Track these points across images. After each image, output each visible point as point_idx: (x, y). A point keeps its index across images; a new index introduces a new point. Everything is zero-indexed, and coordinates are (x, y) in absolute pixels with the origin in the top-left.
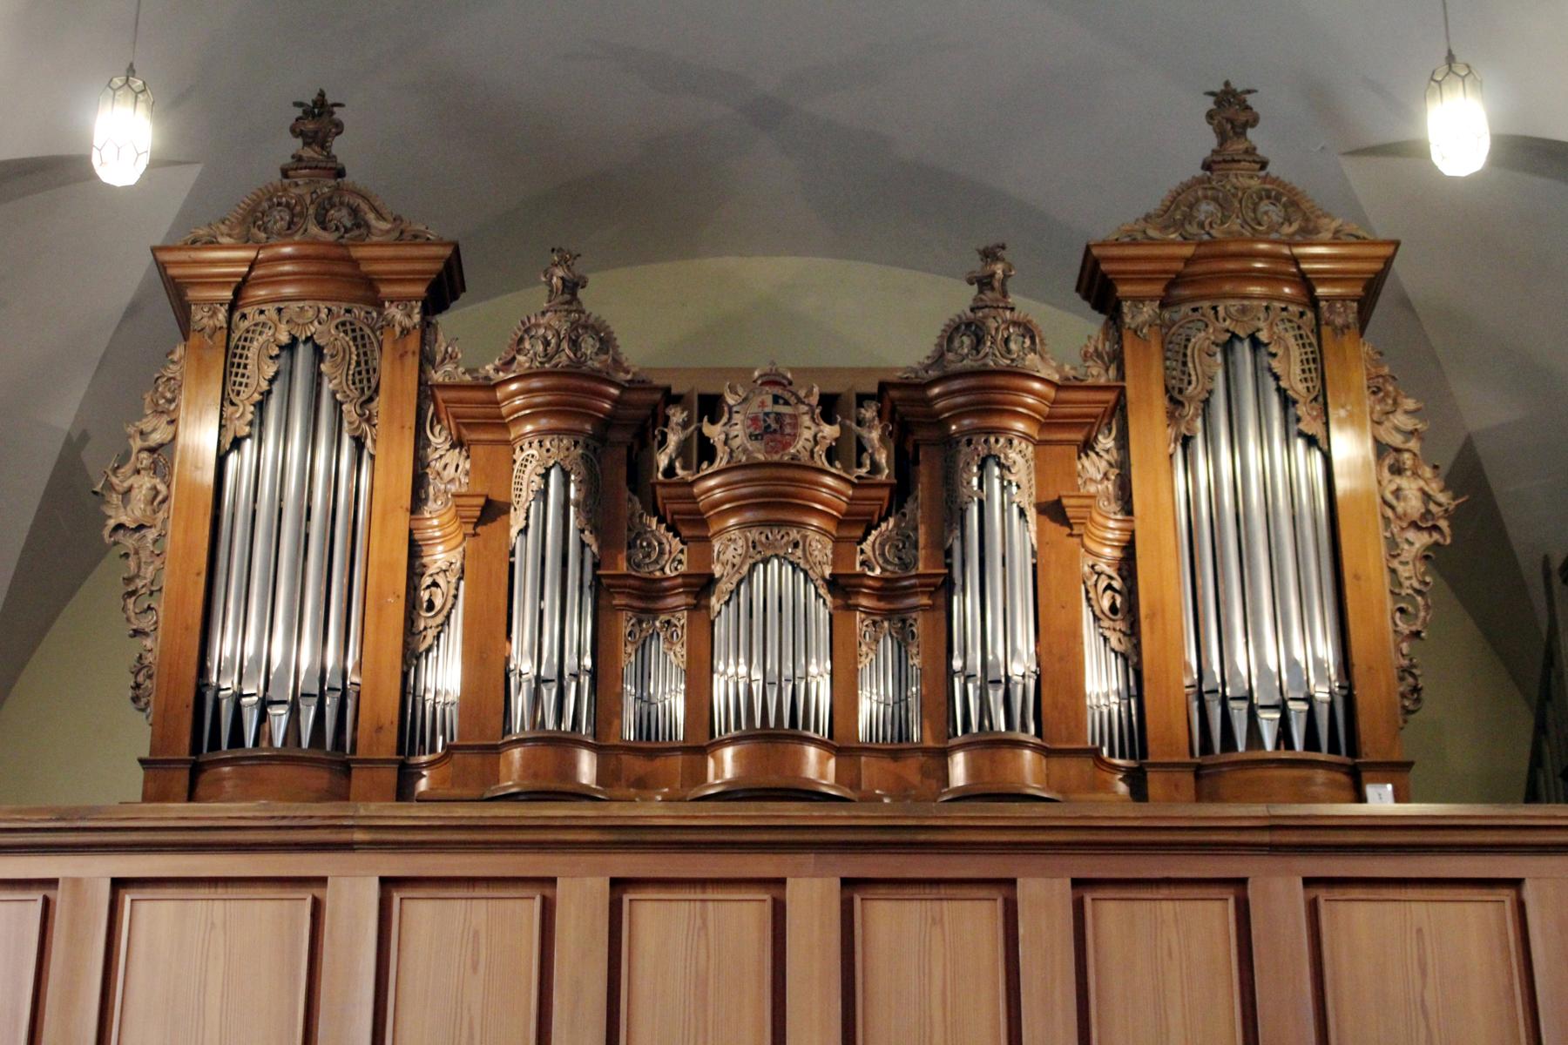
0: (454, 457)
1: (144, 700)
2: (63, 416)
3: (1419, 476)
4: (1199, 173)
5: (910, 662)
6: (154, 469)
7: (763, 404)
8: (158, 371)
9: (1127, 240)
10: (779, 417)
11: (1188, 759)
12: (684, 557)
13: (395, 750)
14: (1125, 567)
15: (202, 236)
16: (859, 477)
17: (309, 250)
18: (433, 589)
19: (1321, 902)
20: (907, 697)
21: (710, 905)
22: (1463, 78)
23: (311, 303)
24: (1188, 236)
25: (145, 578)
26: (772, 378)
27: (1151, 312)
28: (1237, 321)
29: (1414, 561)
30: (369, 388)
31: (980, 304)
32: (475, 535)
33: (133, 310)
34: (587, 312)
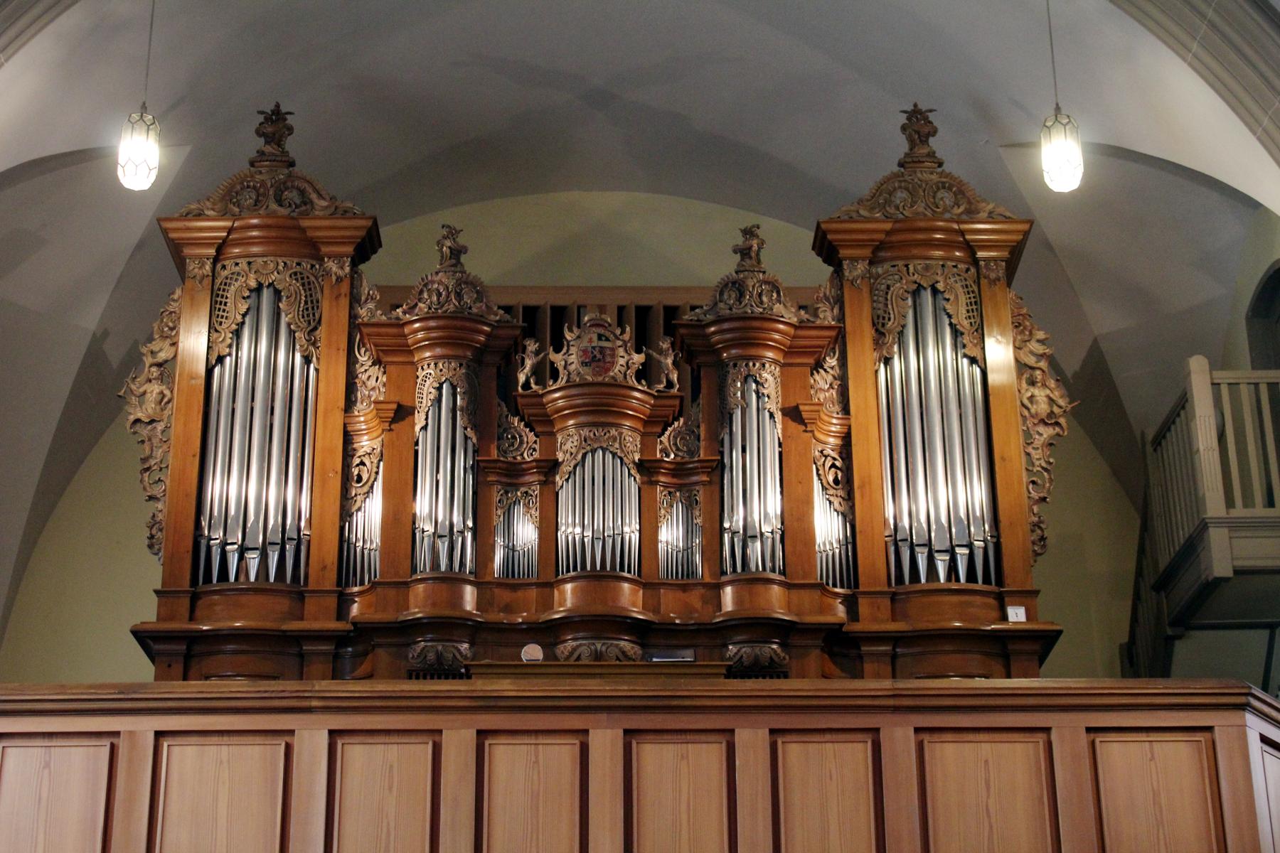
0: (375, 371)
1: (157, 547)
2: (90, 318)
3: (1046, 386)
4: (896, 169)
5: (695, 521)
6: (161, 378)
7: (590, 341)
8: (164, 308)
9: (846, 217)
10: (602, 349)
11: (886, 589)
12: (537, 447)
13: (335, 584)
14: (845, 451)
15: (194, 209)
16: (658, 391)
17: (269, 221)
18: (361, 467)
19: (926, 743)
20: (692, 546)
21: (540, 747)
22: (1065, 126)
23: (272, 258)
24: (889, 215)
25: (156, 458)
26: (598, 322)
27: (863, 268)
28: (922, 275)
29: (1042, 446)
30: (314, 320)
31: (742, 269)
32: (391, 430)
33: (140, 246)
34: (468, 272)
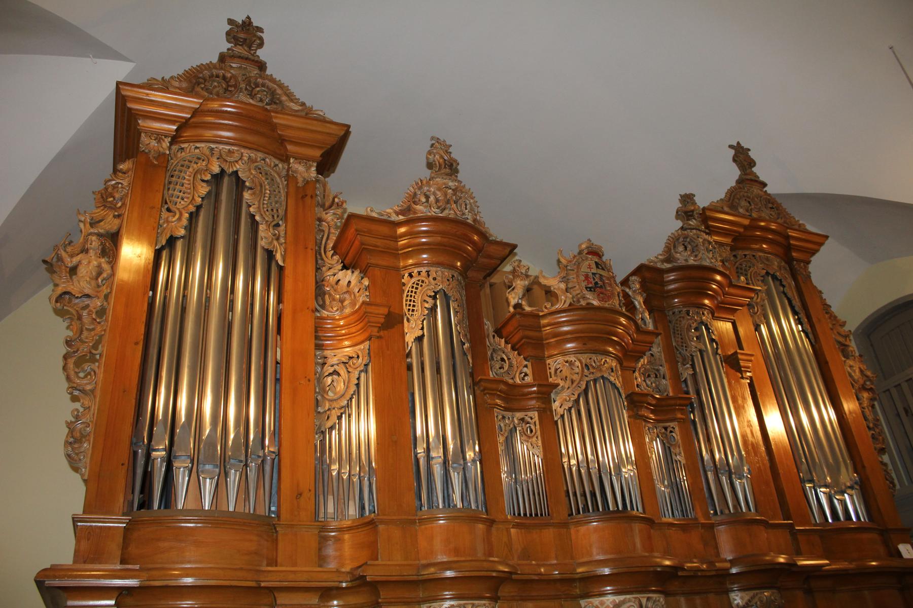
0: (349, 277)
18: (335, 377)
